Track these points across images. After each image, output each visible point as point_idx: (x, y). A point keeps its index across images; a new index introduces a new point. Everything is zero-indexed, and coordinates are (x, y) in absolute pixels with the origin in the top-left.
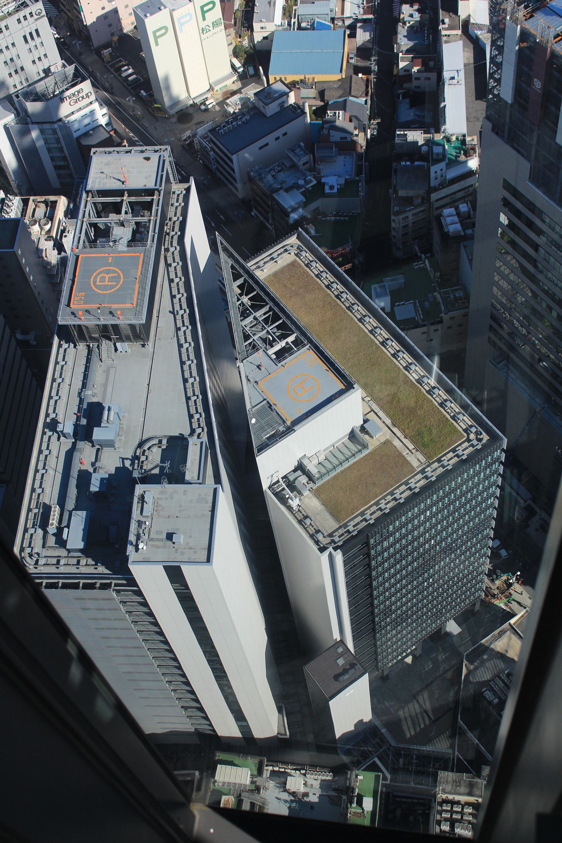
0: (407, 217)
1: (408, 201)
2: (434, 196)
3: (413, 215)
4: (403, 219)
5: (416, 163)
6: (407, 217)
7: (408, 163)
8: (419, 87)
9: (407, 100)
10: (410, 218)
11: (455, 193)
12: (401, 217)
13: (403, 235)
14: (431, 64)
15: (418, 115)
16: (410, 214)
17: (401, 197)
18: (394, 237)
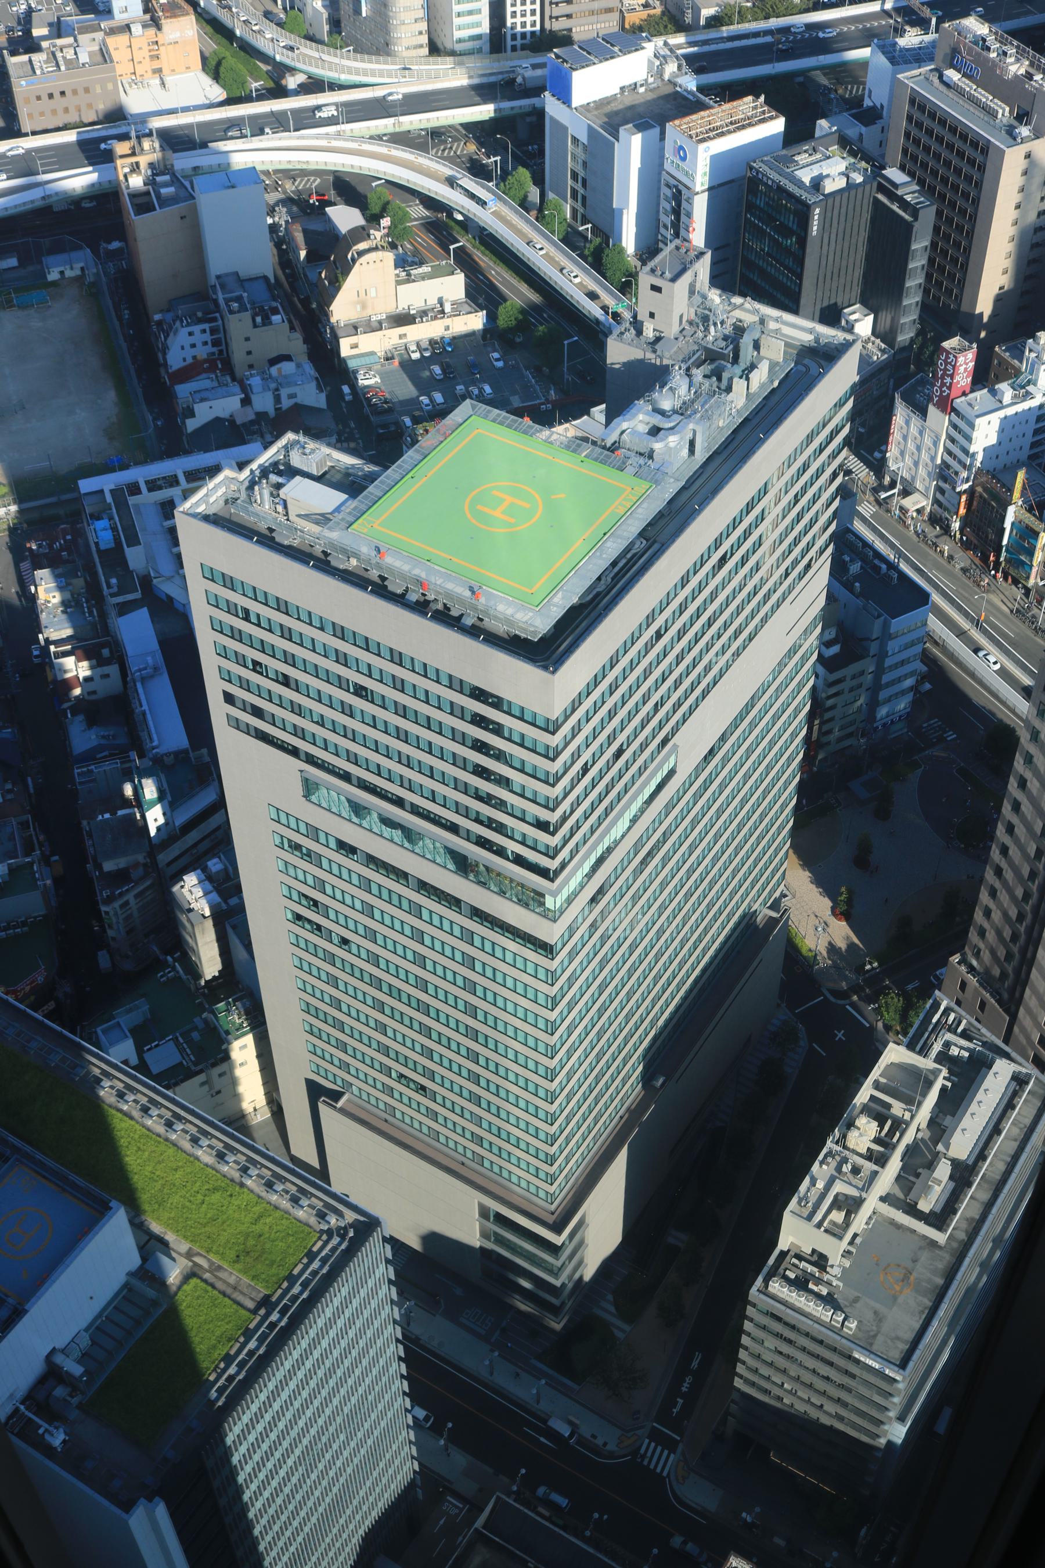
0: (127, 903)
1: (122, 877)
2: (163, 858)
3: (136, 896)
4: (122, 906)
5: (120, 813)
6: (127, 903)
7: (107, 816)
8: (94, 692)
9: (81, 717)
10: (133, 902)
11: (195, 845)
12: (116, 905)
13: (128, 933)
14: (106, 652)
15: (103, 737)
16: (130, 897)
17: (109, 873)
18: (113, 939)
